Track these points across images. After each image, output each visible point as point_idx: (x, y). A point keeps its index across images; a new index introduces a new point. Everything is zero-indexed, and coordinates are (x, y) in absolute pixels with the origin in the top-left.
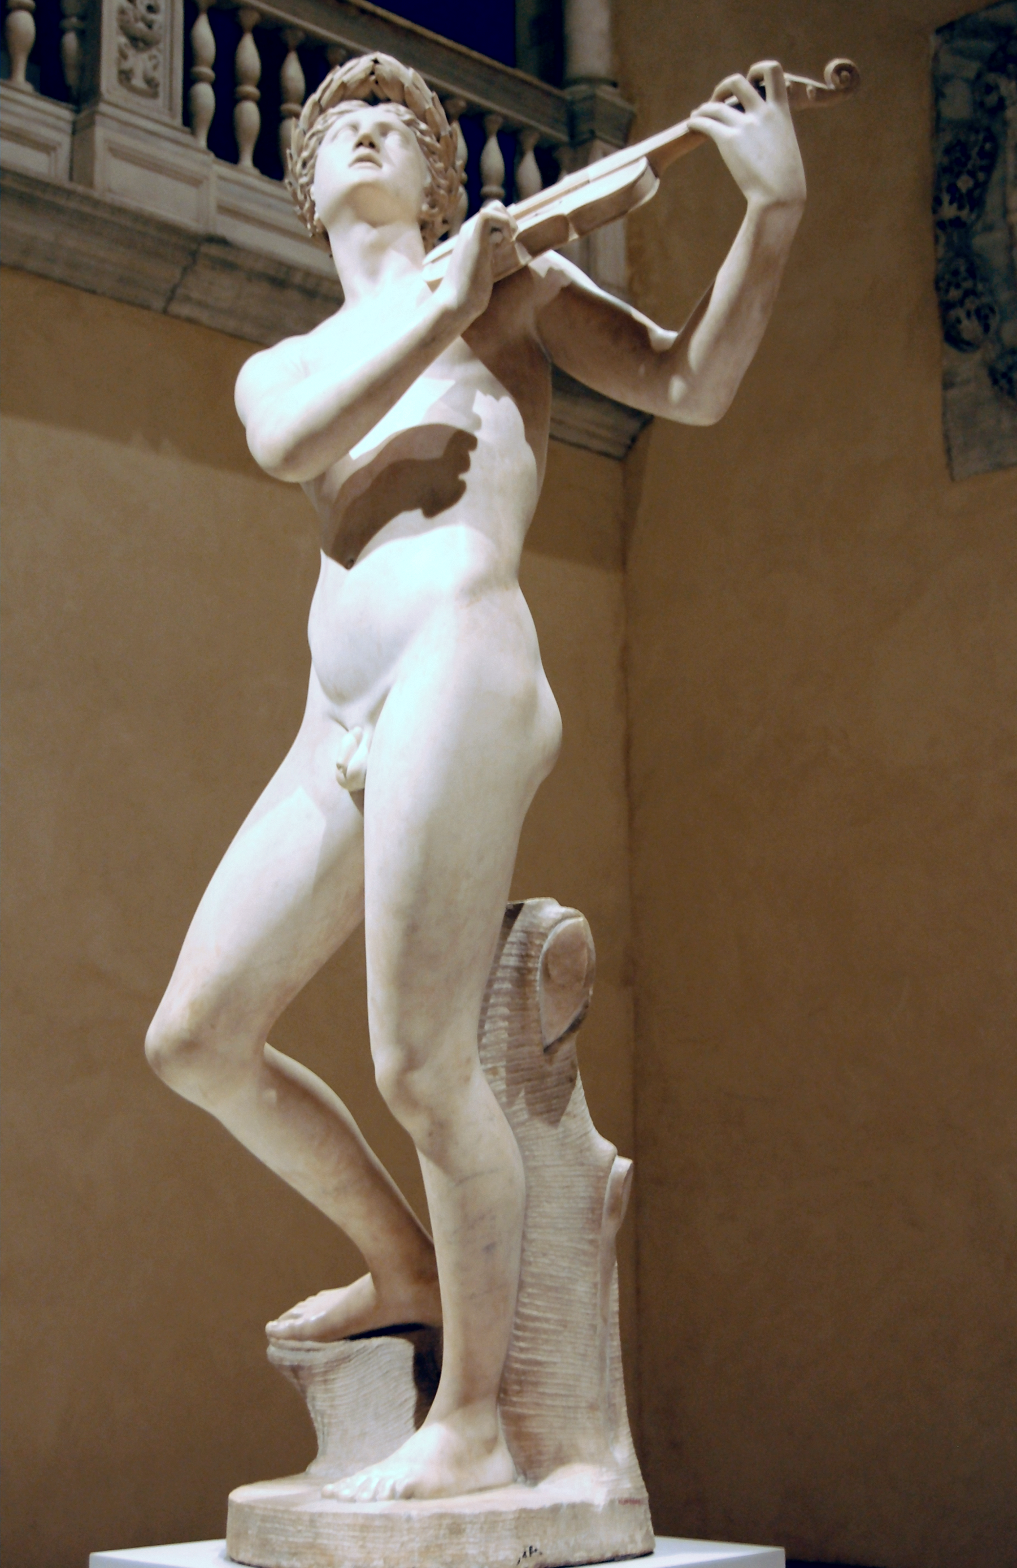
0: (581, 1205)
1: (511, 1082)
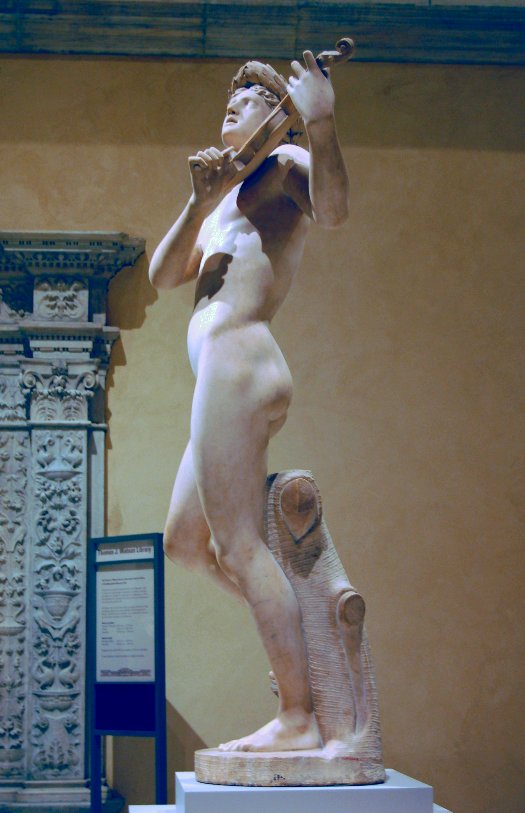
1: (284, 558)
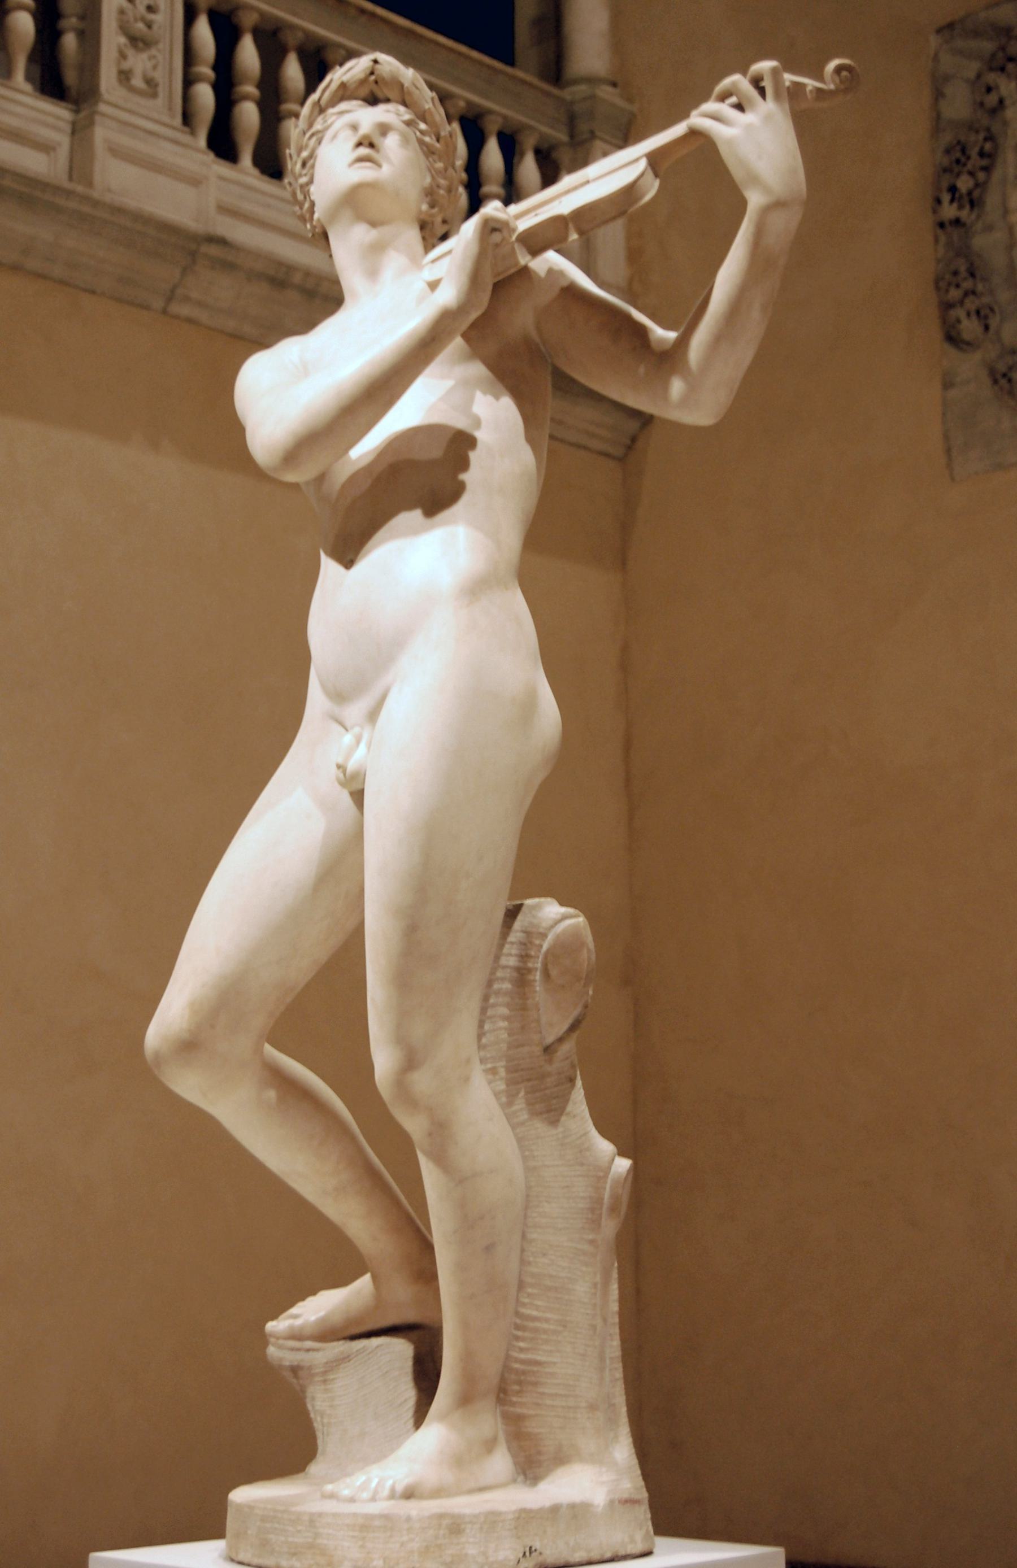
0: (581, 1206)
1: (510, 1082)
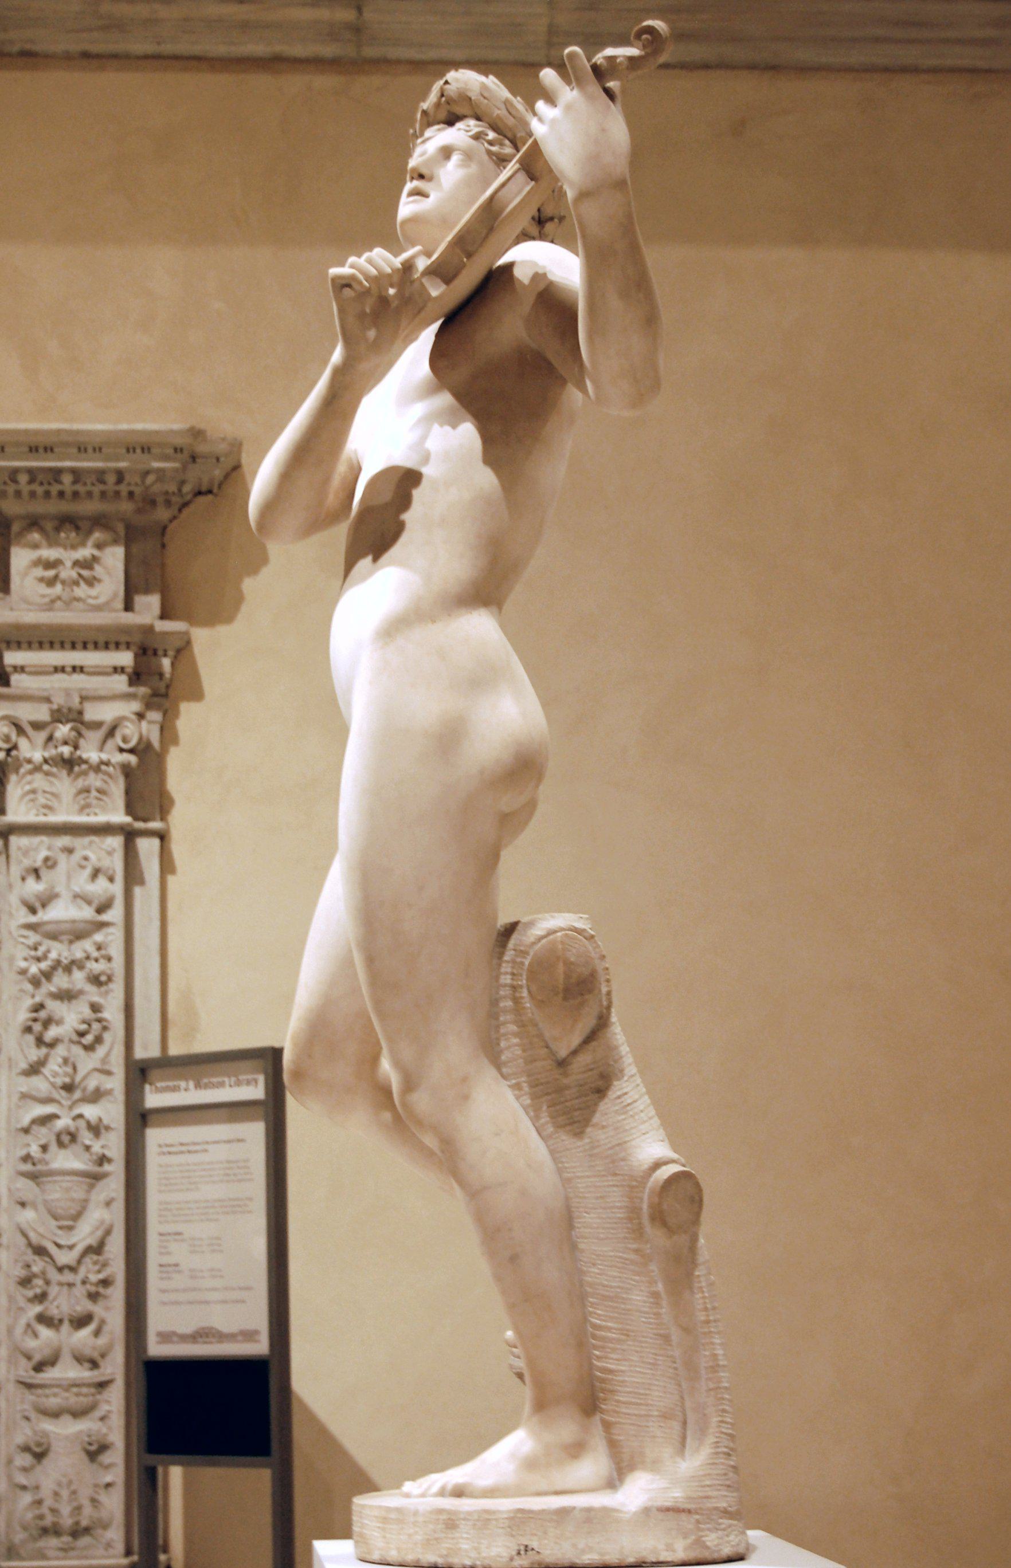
1: (534, 1097)
